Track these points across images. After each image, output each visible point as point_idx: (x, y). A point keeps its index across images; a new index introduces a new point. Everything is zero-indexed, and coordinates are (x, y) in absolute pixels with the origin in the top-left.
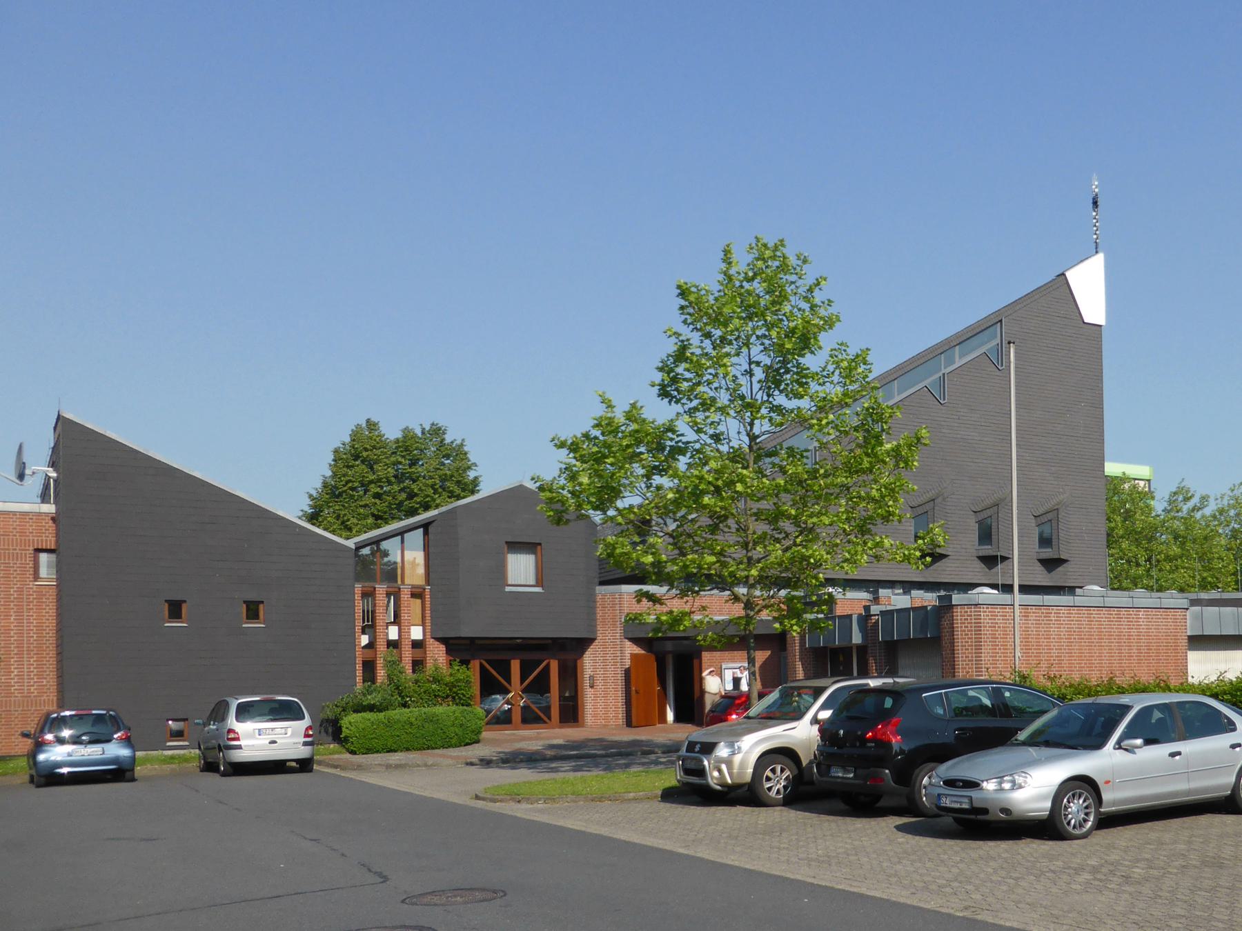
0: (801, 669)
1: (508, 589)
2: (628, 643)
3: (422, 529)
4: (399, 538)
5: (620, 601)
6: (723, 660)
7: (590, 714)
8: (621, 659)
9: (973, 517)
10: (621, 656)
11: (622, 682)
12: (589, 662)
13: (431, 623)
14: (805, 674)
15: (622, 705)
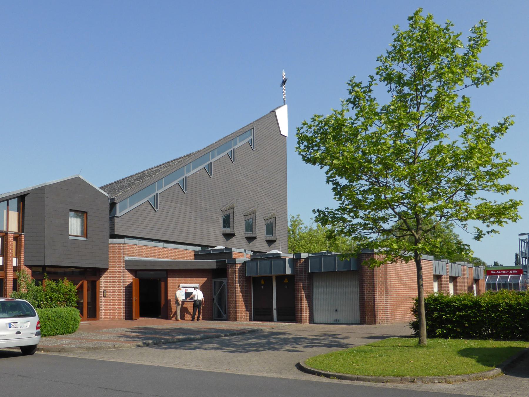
0: (239, 288)
1: (70, 237)
2: (127, 272)
3: (17, 199)
4: (6, 202)
5: (123, 248)
6: (181, 283)
7: (103, 312)
8: (123, 281)
9: (244, 218)
10: (123, 279)
11: (123, 294)
12: (104, 282)
13: (24, 256)
14: (241, 290)
15: (123, 307)
